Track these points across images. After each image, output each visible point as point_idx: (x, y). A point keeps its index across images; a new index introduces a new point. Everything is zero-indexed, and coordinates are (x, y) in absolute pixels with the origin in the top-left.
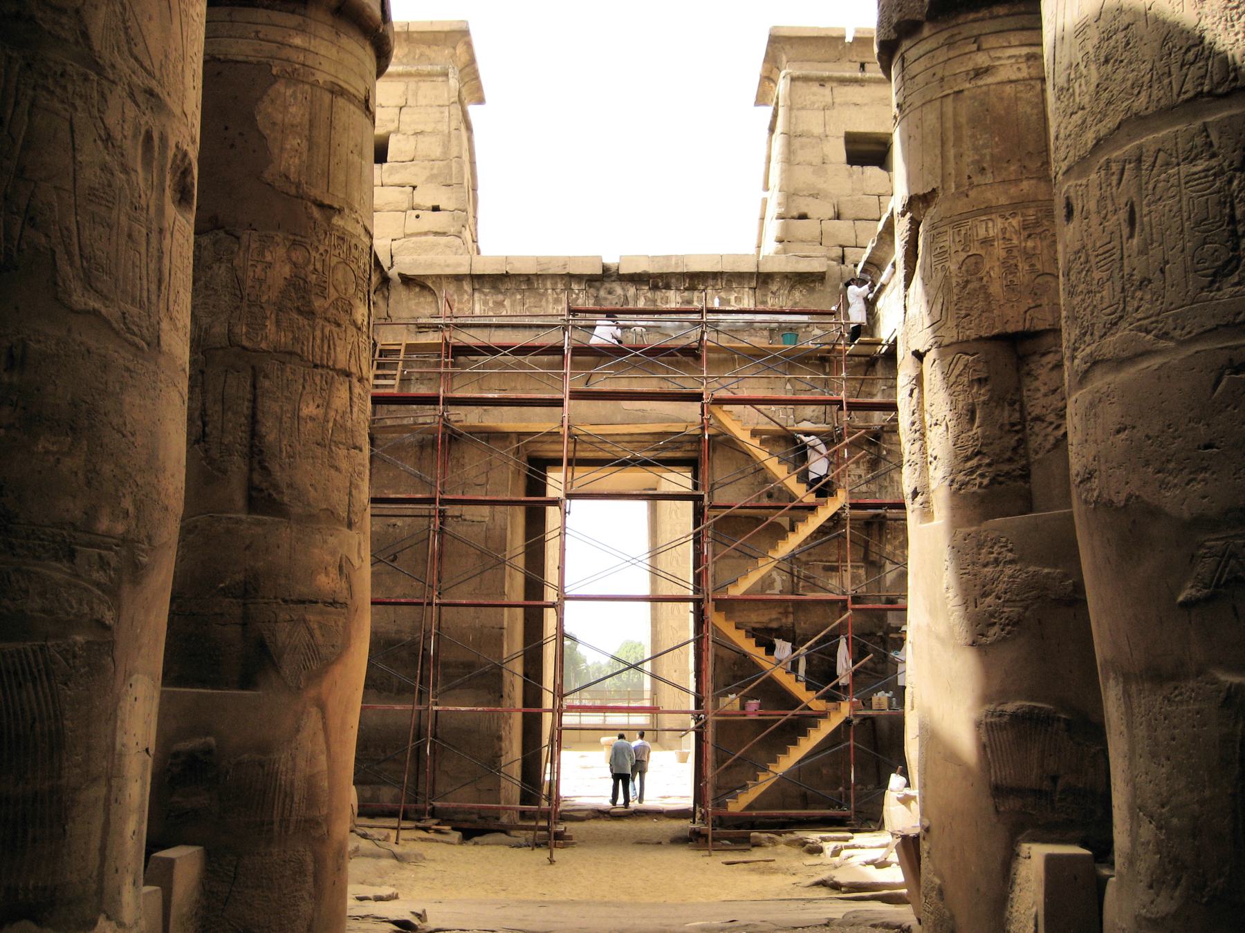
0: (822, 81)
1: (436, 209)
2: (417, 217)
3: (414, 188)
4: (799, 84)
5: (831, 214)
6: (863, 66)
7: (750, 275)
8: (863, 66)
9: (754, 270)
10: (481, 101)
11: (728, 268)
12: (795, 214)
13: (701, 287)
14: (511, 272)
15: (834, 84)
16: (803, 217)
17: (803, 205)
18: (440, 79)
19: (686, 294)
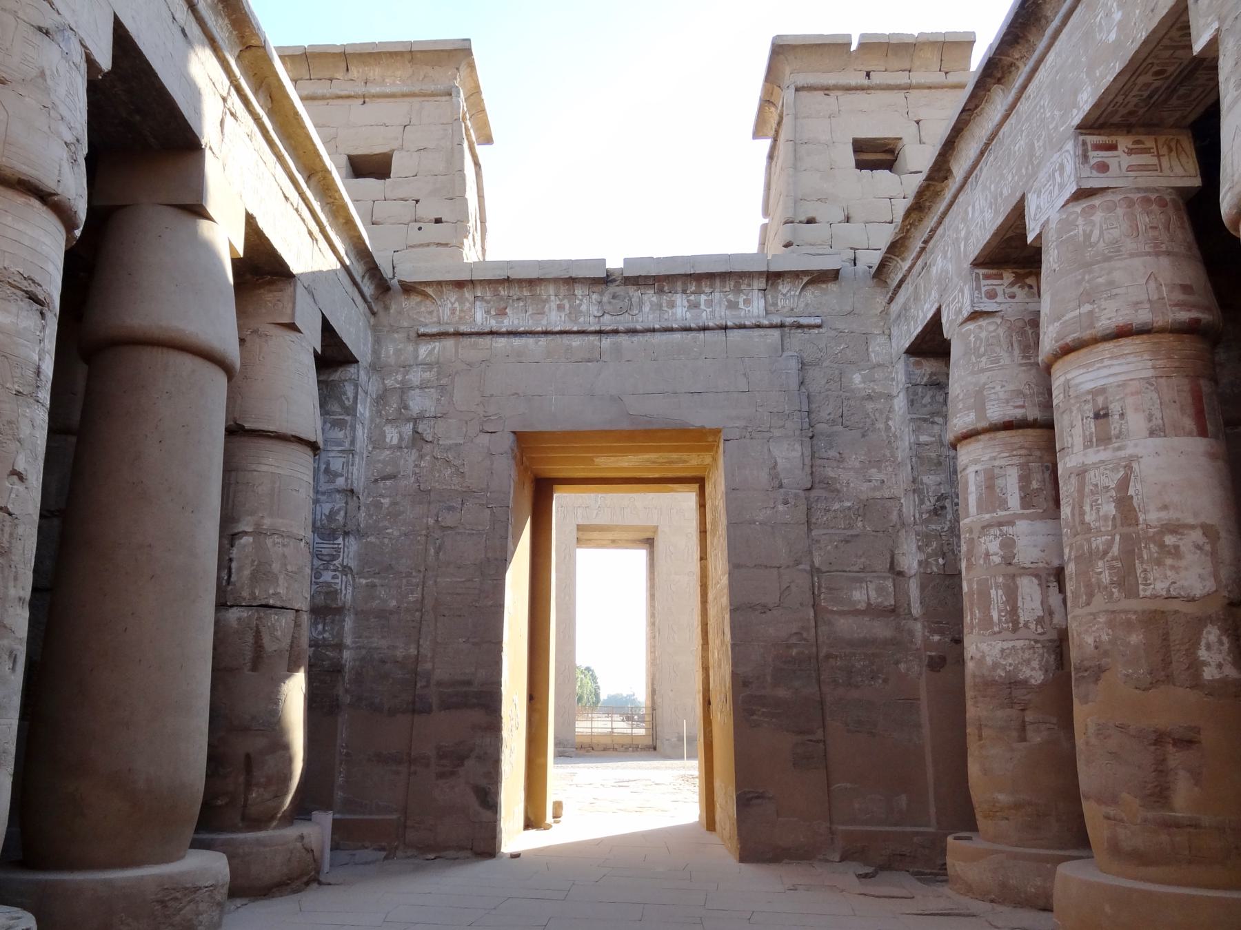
0: (826, 89)
1: (438, 221)
2: (420, 229)
3: (417, 201)
4: (801, 93)
5: (842, 218)
6: (868, 74)
7: (760, 273)
8: (868, 74)
9: (765, 269)
10: (488, 140)
11: (737, 269)
12: (804, 218)
13: (708, 290)
14: (513, 277)
15: (839, 93)
16: (811, 221)
17: (809, 210)
18: (444, 99)
19: (692, 298)
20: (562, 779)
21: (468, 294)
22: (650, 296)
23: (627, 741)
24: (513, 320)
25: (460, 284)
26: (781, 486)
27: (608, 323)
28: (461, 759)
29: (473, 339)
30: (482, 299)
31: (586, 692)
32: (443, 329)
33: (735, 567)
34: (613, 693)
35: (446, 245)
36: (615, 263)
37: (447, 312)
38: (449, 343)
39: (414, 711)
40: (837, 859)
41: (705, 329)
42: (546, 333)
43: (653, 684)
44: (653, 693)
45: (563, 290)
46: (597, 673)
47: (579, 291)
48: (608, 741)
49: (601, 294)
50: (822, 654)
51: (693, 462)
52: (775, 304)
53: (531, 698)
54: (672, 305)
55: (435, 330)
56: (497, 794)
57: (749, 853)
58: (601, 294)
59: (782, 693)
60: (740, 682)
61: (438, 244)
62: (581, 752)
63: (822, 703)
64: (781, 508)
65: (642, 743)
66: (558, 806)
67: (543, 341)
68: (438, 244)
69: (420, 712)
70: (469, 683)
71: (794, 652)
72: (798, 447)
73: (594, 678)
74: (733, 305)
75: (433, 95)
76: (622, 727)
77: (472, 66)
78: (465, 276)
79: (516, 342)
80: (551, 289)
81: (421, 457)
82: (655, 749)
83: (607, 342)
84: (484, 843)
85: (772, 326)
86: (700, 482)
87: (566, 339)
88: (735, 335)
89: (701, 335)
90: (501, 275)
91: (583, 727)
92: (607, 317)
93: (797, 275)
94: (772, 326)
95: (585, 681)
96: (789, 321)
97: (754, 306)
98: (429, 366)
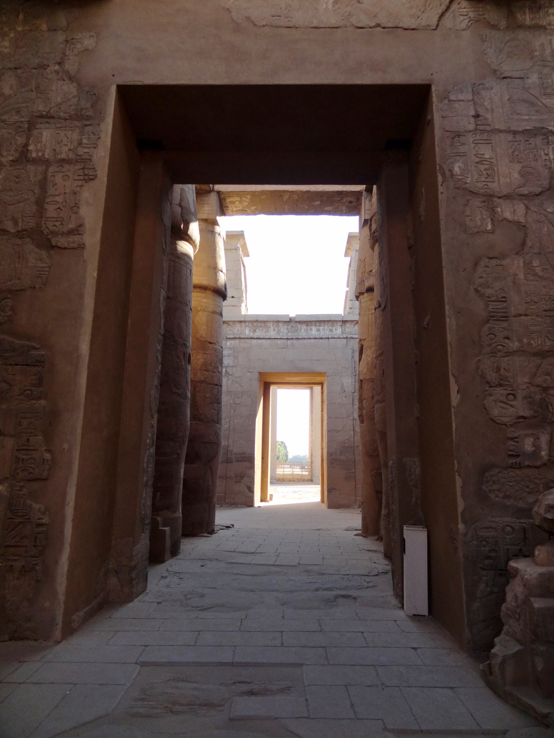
7: (340, 321)
11: (333, 319)
20: (271, 489)
21: (243, 324)
22: (304, 327)
23: (300, 477)
24: (258, 334)
25: (241, 322)
26: (344, 392)
27: (290, 335)
28: (242, 477)
29: (245, 340)
30: (248, 326)
31: (281, 454)
32: (235, 336)
33: (329, 418)
34: (295, 455)
35: (235, 306)
36: (292, 315)
37: (236, 330)
38: (237, 341)
39: (227, 462)
40: (357, 507)
41: (321, 338)
42: (269, 339)
43: (311, 452)
44: (312, 455)
45: (275, 324)
46: (287, 445)
47: (280, 324)
48: (291, 477)
49: (288, 326)
50: (355, 446)
51: (319, 379)
52: (345, 330)
53: (263, 458)
54: (311, 330)
55: (232, 337)
56: (253, 488)
57: (330, 506)
58: (288, 326)
59: (343, 458)
60: (330, 454)
61: (233, 306)
62: (279, 482)
63: (355, 461)
64: (344, 398)
65: (306, 478)
66: (271, 496)
67: (268, 341)
68: (233, 306)
69: (230, 462)
70: (244, 454)
71: (347, 445)
72: (350, 379)
73: (285, 447)
74: (331, 330)
75: (231, 249)
76: (297, 471)
77: (244, 239)
78: (242, 319)
79: (259, 341)
80: (271, 324)
81: (228, 380)
82: (312, 481)
83: (289, 342)
84: (250, 503)
85: (343, 338)
86: (322, 384)
87: (276, 341)
88: (331, 341)
89: (320, 340)
90: (254, 319)
91: (280, 471)
92: (290, 333)
93: (352, 321)
94: (343, 338)
95: (281, 448)
96: (349, 336)
97: (338, 331)
98: (230, 349)
